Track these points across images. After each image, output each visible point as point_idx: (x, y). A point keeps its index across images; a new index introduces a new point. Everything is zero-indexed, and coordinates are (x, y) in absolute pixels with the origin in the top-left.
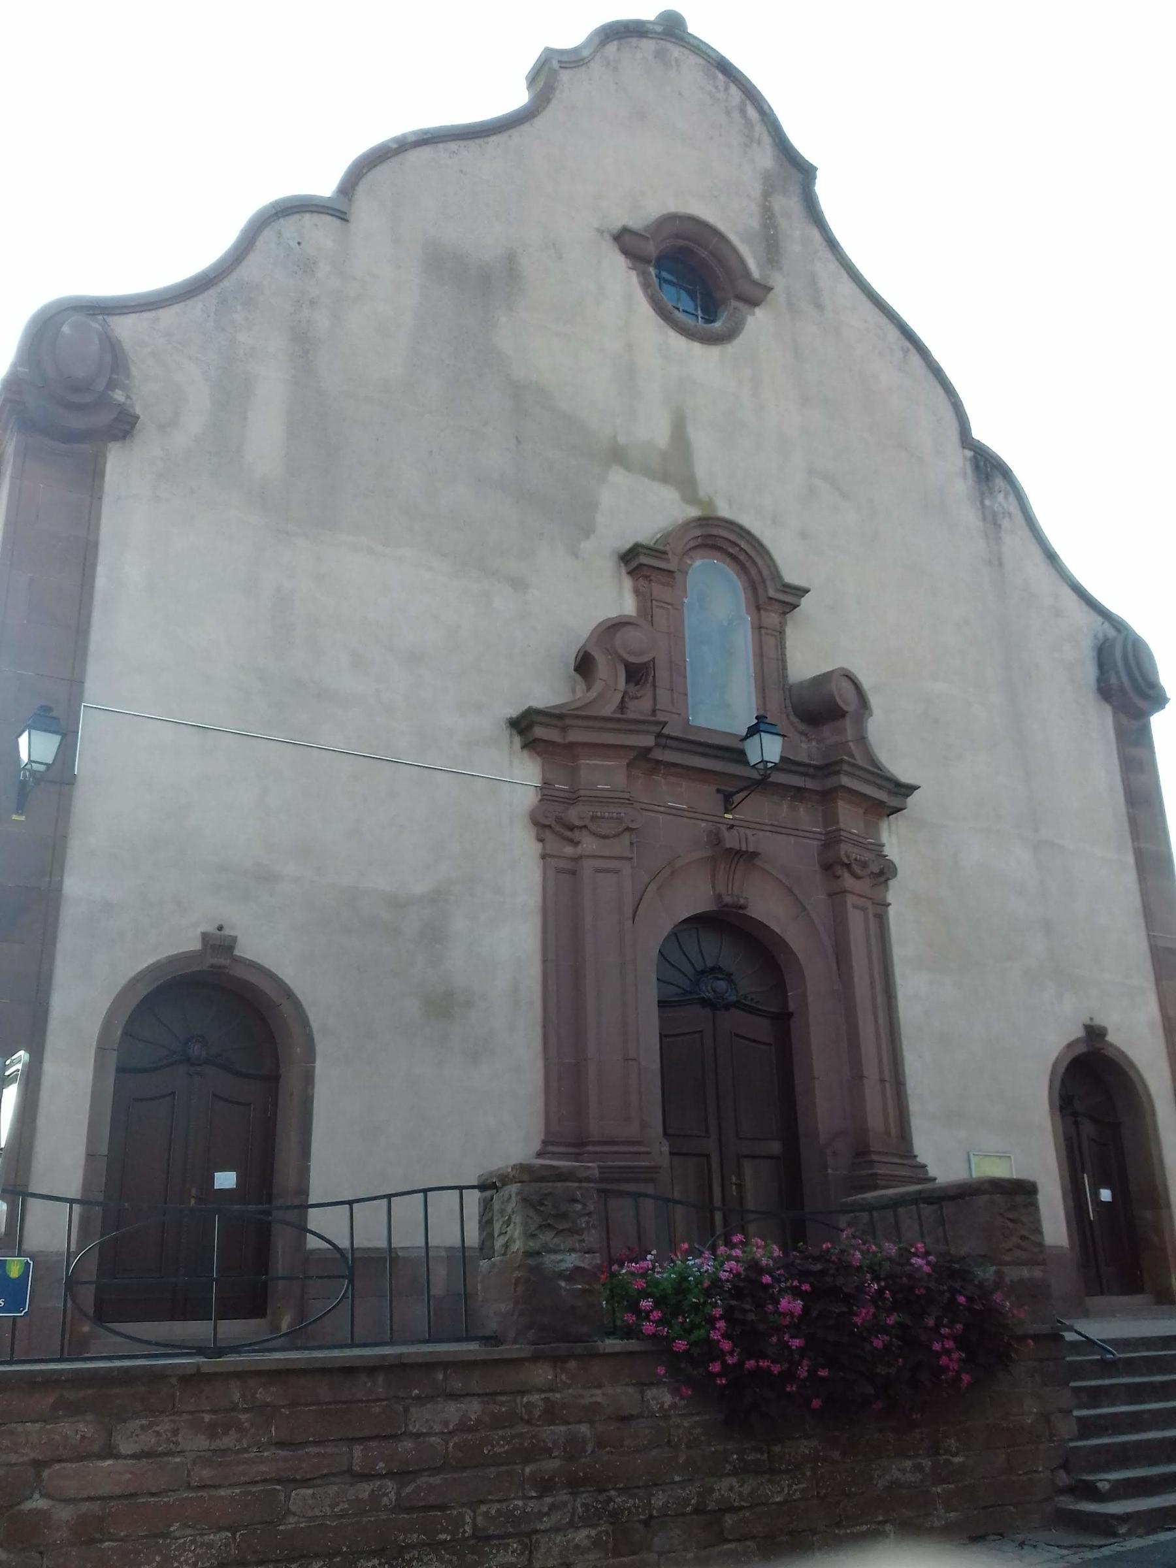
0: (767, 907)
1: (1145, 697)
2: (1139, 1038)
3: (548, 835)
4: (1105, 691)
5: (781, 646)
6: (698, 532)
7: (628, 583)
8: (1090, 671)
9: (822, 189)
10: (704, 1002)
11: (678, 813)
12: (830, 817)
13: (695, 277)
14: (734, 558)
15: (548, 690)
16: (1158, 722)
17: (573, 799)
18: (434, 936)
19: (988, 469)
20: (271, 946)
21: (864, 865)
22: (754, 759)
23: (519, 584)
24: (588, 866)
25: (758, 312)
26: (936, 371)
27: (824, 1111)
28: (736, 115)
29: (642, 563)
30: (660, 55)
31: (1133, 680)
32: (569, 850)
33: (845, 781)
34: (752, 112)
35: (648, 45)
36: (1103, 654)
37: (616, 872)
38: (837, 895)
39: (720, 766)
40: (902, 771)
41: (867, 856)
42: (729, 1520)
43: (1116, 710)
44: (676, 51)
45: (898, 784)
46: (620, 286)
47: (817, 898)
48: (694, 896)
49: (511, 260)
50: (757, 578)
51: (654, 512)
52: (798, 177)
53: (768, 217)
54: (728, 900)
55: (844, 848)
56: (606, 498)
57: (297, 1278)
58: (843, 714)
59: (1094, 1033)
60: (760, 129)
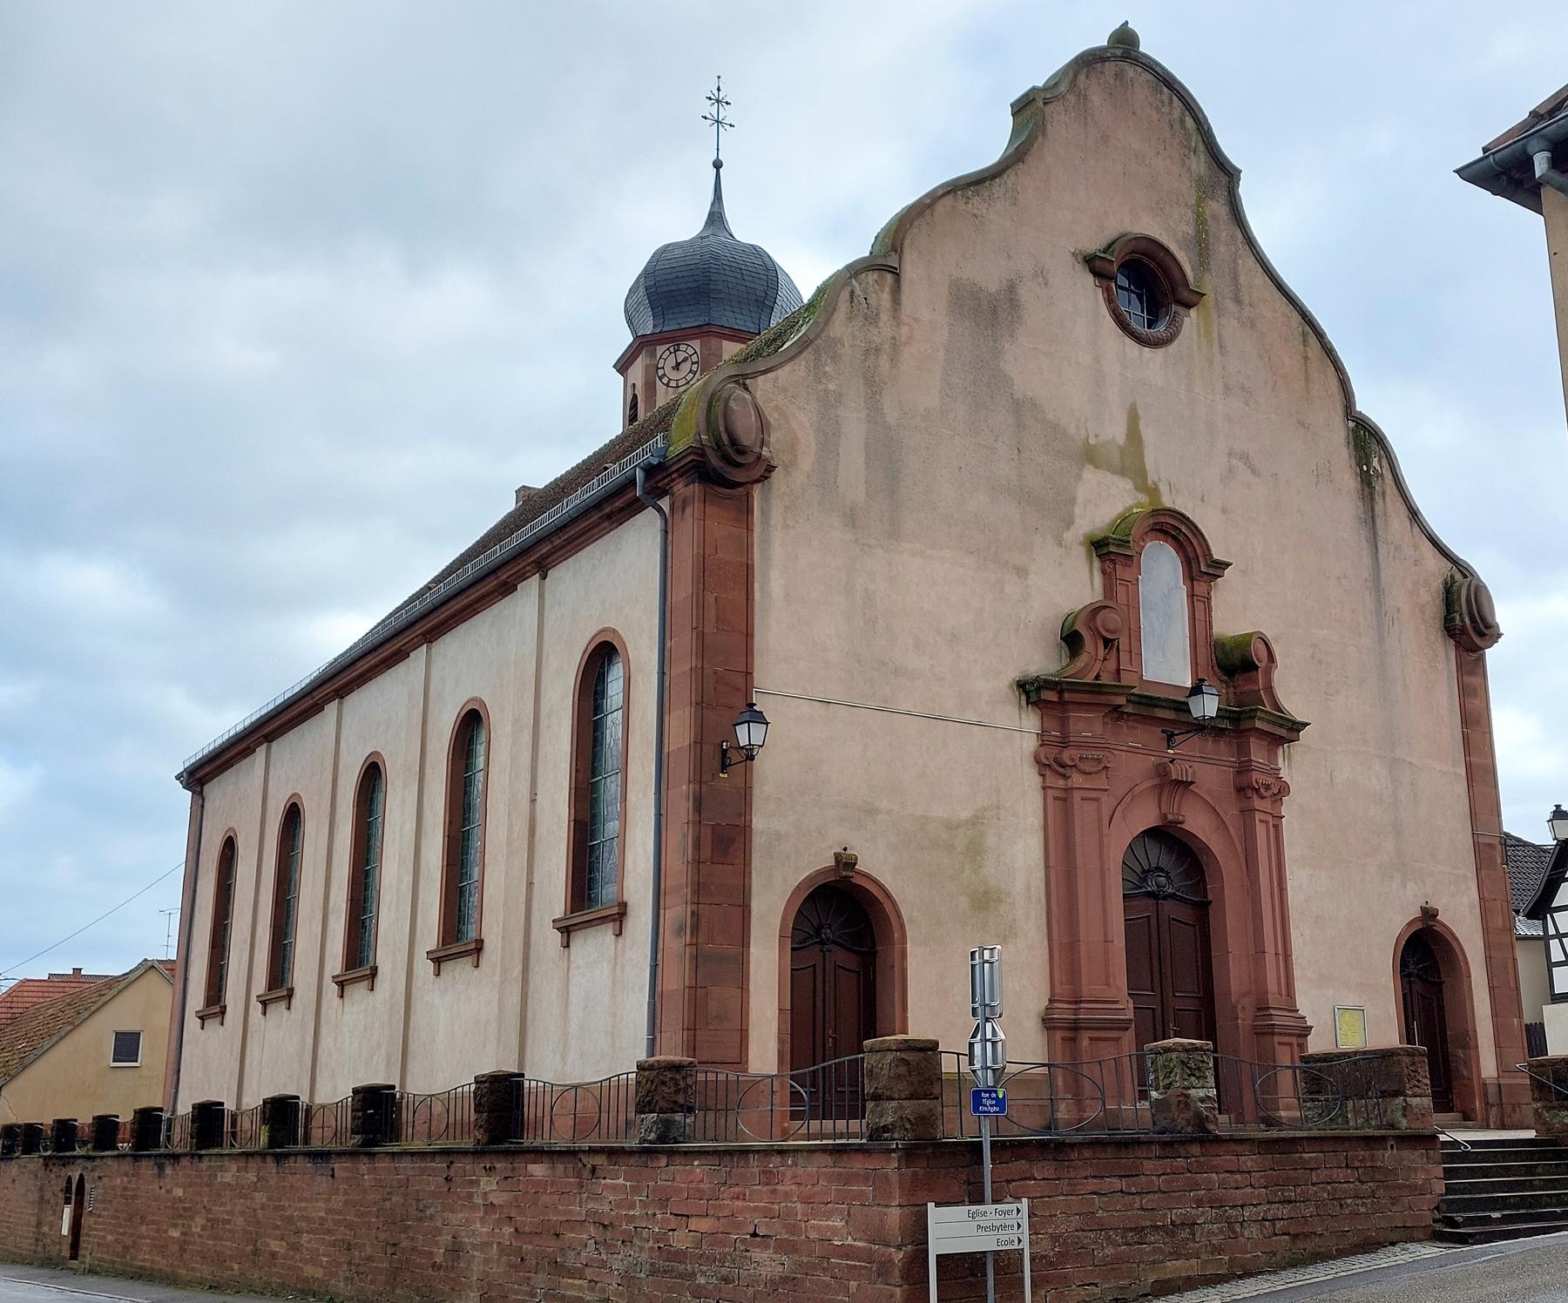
0: (1197, 823)
1: (1481, 635)
2: (1464, 922)
3: (1048, 773)
4: (1451, 629)
5: (1208, 610)
6: (1151, 521)
7: (1097, 563)
8: (1435, 609)
9: (1245, 190)
10: (1149, 894)
11: (1134, 755)
12: (1243, 750)
13: (1146, 285)
14: (1174, 537)
15: (1042, 661)
16: (1491, 654)
17: (1064, 743)
18: (975, 851)
19: (1366, 440)
20: (878, 864)
21: (1268, 787)
22: (1196, 713)
23: (1022, 572)
24: (1077, 795)
25: (1193, 312)
26: (1329, 352)
27: (1234, 976)
28: (1177, 126)
29: (1111, 551)
30: (1119, 76)
31: (1473, 620)
32: (1061, 783)
33: (1258, 724)
34: (1189, 122)
35: (1110, 68)
36: (1449, 594)
37: (1097, 800)
38: (1247, 813)
39: (1163, 713)
40: (1294, 703)
41: (1270, 780)
42: (1279, 1224)
43: (1458, 645)
44: (1131, 71)
45: (1294, 722)
46: (1086, 295)
47: (1230, 813)
48: (1146, 816)
49: (1297, 727)
50: (1192, 555)
51: (1105, 501)
52: (1224, 179)
53: (1200, 221)
54: (1170, 817)
55: (1255, 775)
56: (1082, 493)
57: (1081, 1109)
58: (1257, 668)
59: (1429, 914)
60: (1196, 140)
